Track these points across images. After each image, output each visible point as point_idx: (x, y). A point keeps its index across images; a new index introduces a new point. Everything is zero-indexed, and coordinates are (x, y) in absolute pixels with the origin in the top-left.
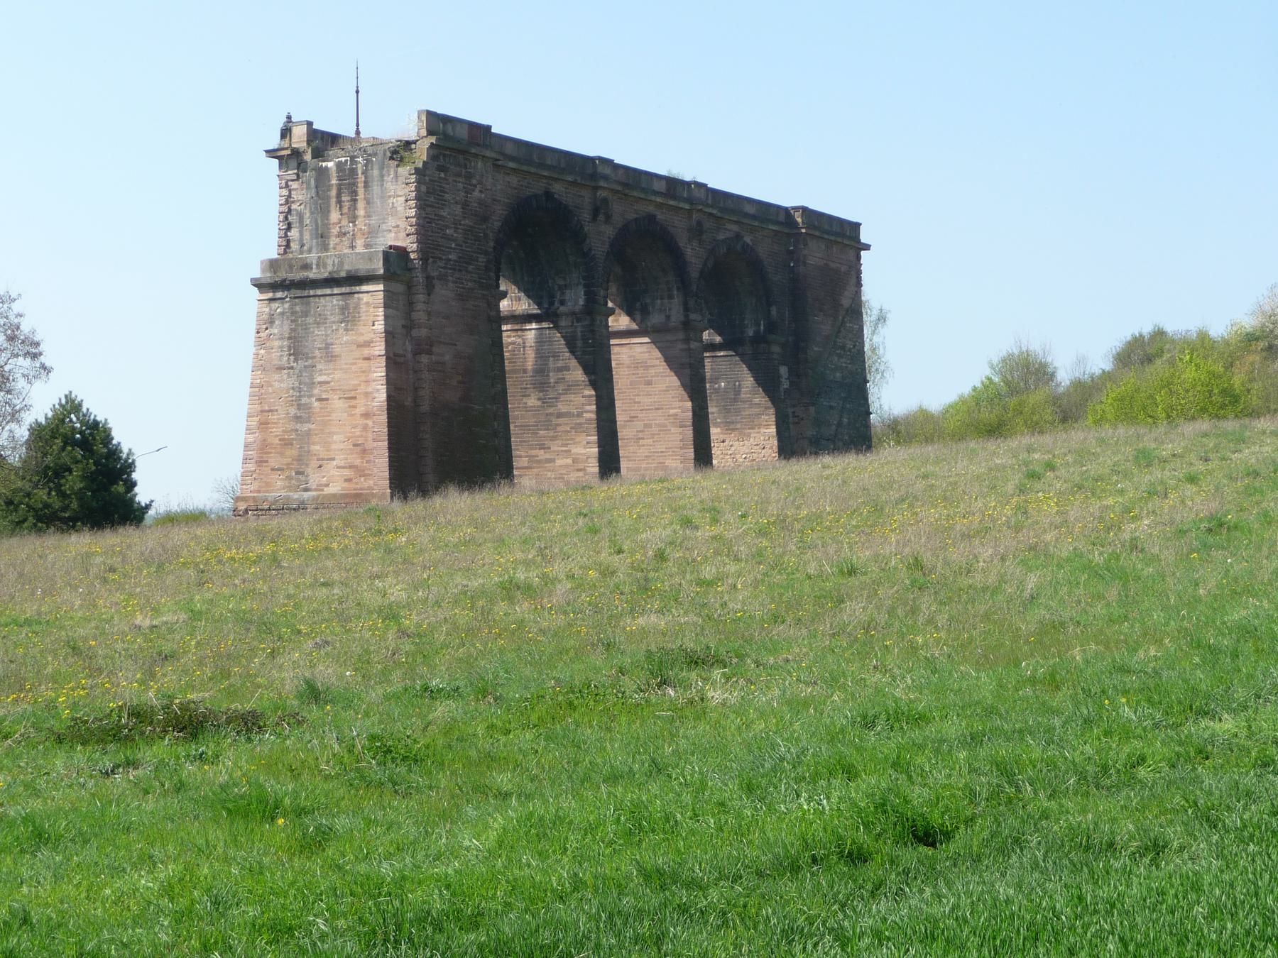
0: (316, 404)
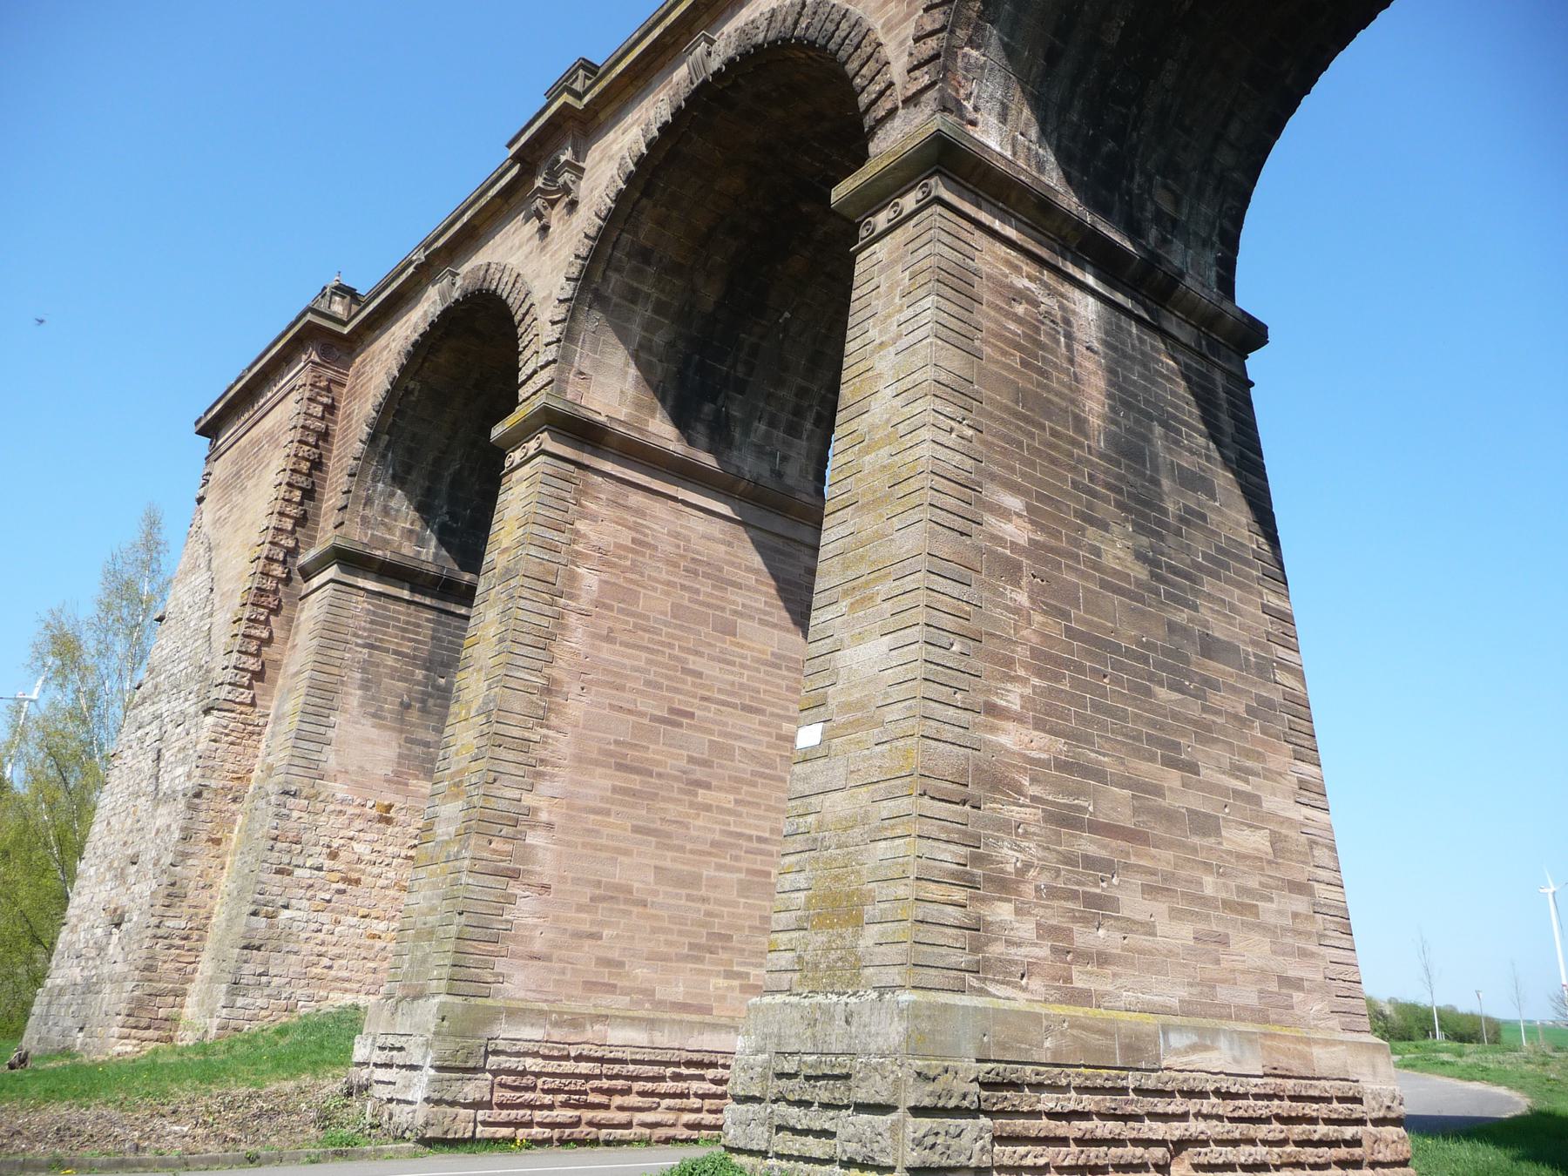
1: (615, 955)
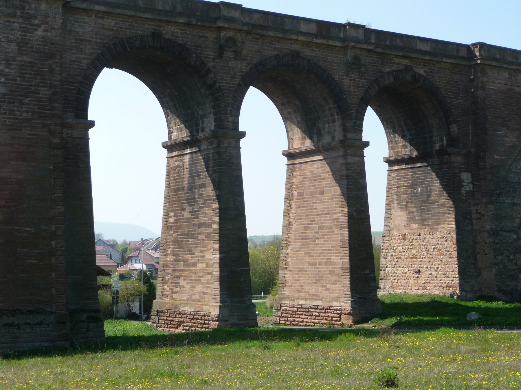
1: (302, 284)
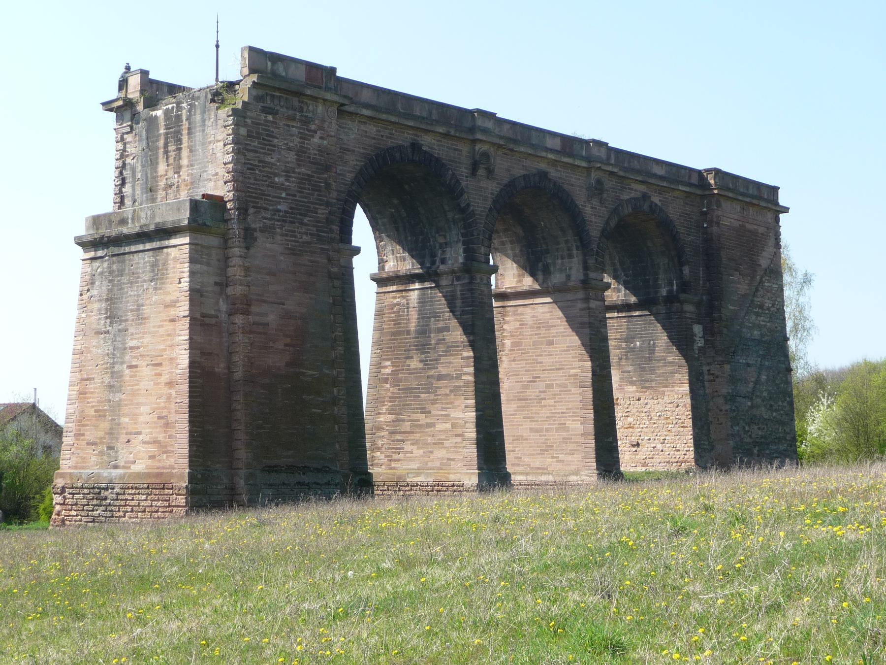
0: (127, 372)
1: (519, 455)
